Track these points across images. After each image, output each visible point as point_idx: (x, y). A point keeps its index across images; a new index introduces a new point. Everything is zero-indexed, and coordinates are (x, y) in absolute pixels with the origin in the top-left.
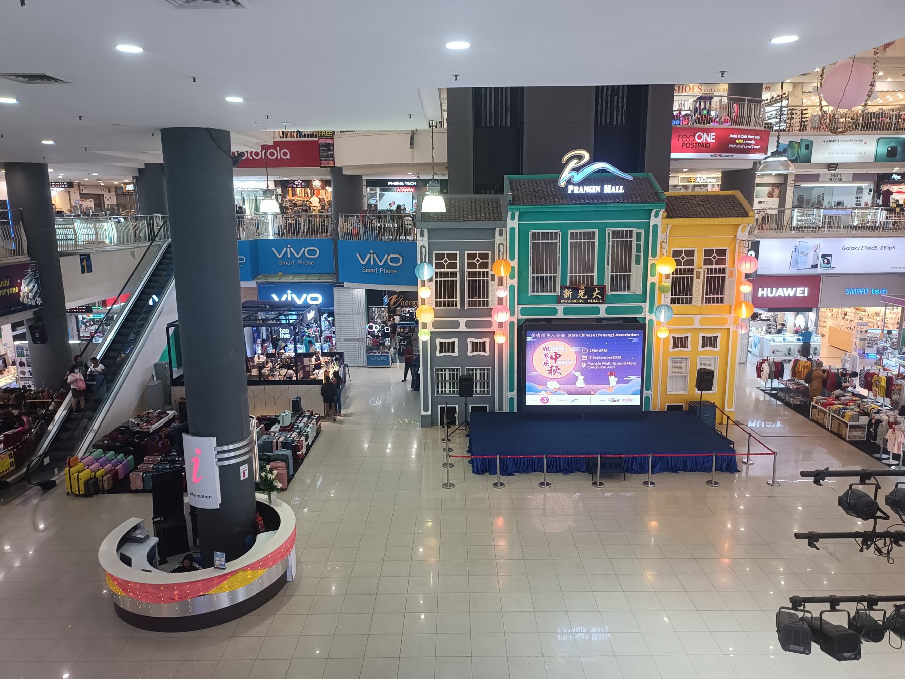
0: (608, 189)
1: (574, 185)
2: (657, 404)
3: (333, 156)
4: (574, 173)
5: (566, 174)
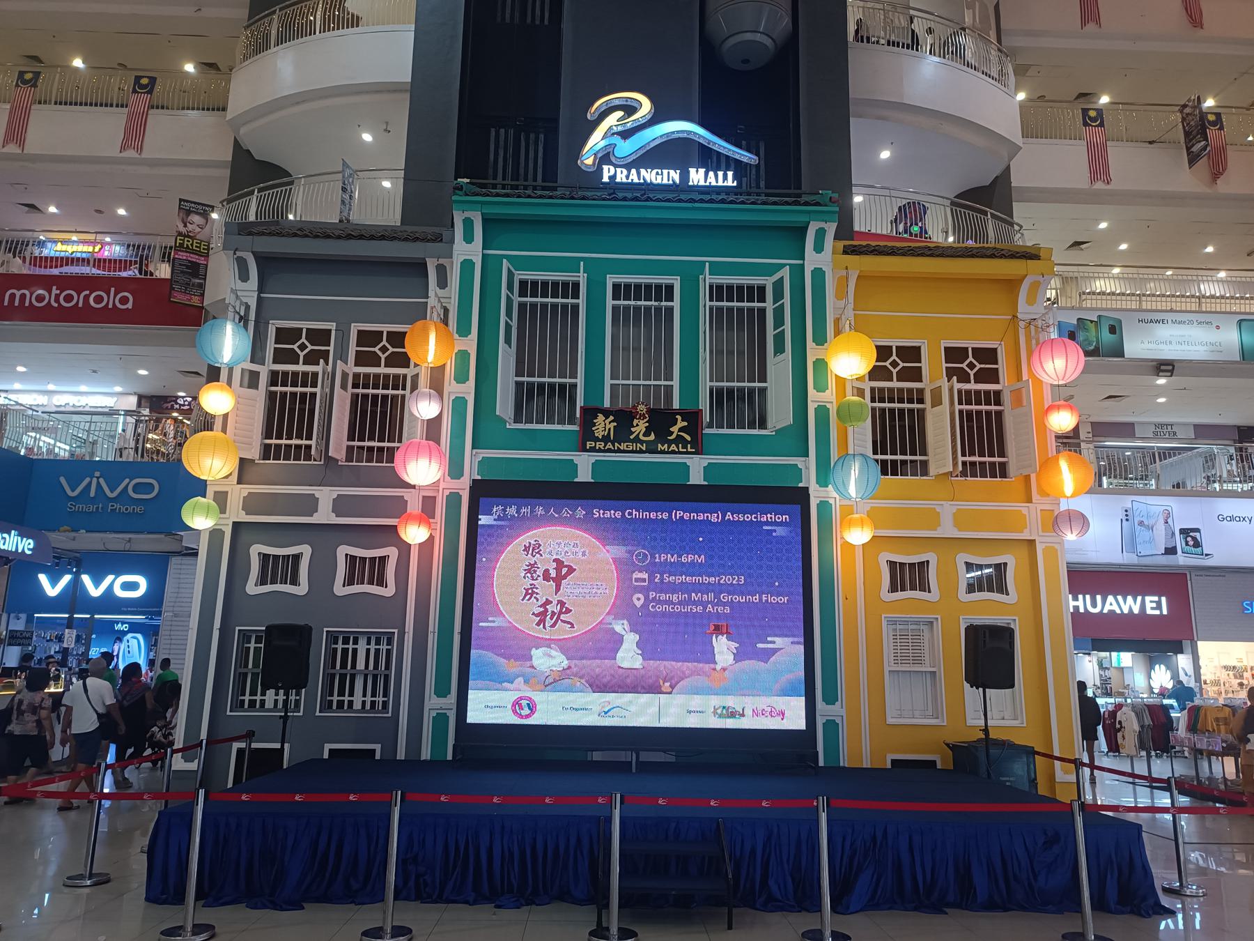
0: (697, 177)
1: (616, 166)
2: (860, 748)
3: (202, 287)
4: (617, 140)
5: (596, 140)
